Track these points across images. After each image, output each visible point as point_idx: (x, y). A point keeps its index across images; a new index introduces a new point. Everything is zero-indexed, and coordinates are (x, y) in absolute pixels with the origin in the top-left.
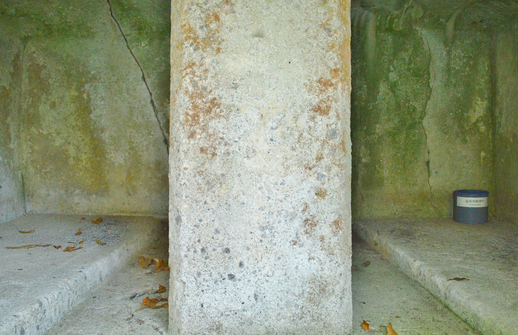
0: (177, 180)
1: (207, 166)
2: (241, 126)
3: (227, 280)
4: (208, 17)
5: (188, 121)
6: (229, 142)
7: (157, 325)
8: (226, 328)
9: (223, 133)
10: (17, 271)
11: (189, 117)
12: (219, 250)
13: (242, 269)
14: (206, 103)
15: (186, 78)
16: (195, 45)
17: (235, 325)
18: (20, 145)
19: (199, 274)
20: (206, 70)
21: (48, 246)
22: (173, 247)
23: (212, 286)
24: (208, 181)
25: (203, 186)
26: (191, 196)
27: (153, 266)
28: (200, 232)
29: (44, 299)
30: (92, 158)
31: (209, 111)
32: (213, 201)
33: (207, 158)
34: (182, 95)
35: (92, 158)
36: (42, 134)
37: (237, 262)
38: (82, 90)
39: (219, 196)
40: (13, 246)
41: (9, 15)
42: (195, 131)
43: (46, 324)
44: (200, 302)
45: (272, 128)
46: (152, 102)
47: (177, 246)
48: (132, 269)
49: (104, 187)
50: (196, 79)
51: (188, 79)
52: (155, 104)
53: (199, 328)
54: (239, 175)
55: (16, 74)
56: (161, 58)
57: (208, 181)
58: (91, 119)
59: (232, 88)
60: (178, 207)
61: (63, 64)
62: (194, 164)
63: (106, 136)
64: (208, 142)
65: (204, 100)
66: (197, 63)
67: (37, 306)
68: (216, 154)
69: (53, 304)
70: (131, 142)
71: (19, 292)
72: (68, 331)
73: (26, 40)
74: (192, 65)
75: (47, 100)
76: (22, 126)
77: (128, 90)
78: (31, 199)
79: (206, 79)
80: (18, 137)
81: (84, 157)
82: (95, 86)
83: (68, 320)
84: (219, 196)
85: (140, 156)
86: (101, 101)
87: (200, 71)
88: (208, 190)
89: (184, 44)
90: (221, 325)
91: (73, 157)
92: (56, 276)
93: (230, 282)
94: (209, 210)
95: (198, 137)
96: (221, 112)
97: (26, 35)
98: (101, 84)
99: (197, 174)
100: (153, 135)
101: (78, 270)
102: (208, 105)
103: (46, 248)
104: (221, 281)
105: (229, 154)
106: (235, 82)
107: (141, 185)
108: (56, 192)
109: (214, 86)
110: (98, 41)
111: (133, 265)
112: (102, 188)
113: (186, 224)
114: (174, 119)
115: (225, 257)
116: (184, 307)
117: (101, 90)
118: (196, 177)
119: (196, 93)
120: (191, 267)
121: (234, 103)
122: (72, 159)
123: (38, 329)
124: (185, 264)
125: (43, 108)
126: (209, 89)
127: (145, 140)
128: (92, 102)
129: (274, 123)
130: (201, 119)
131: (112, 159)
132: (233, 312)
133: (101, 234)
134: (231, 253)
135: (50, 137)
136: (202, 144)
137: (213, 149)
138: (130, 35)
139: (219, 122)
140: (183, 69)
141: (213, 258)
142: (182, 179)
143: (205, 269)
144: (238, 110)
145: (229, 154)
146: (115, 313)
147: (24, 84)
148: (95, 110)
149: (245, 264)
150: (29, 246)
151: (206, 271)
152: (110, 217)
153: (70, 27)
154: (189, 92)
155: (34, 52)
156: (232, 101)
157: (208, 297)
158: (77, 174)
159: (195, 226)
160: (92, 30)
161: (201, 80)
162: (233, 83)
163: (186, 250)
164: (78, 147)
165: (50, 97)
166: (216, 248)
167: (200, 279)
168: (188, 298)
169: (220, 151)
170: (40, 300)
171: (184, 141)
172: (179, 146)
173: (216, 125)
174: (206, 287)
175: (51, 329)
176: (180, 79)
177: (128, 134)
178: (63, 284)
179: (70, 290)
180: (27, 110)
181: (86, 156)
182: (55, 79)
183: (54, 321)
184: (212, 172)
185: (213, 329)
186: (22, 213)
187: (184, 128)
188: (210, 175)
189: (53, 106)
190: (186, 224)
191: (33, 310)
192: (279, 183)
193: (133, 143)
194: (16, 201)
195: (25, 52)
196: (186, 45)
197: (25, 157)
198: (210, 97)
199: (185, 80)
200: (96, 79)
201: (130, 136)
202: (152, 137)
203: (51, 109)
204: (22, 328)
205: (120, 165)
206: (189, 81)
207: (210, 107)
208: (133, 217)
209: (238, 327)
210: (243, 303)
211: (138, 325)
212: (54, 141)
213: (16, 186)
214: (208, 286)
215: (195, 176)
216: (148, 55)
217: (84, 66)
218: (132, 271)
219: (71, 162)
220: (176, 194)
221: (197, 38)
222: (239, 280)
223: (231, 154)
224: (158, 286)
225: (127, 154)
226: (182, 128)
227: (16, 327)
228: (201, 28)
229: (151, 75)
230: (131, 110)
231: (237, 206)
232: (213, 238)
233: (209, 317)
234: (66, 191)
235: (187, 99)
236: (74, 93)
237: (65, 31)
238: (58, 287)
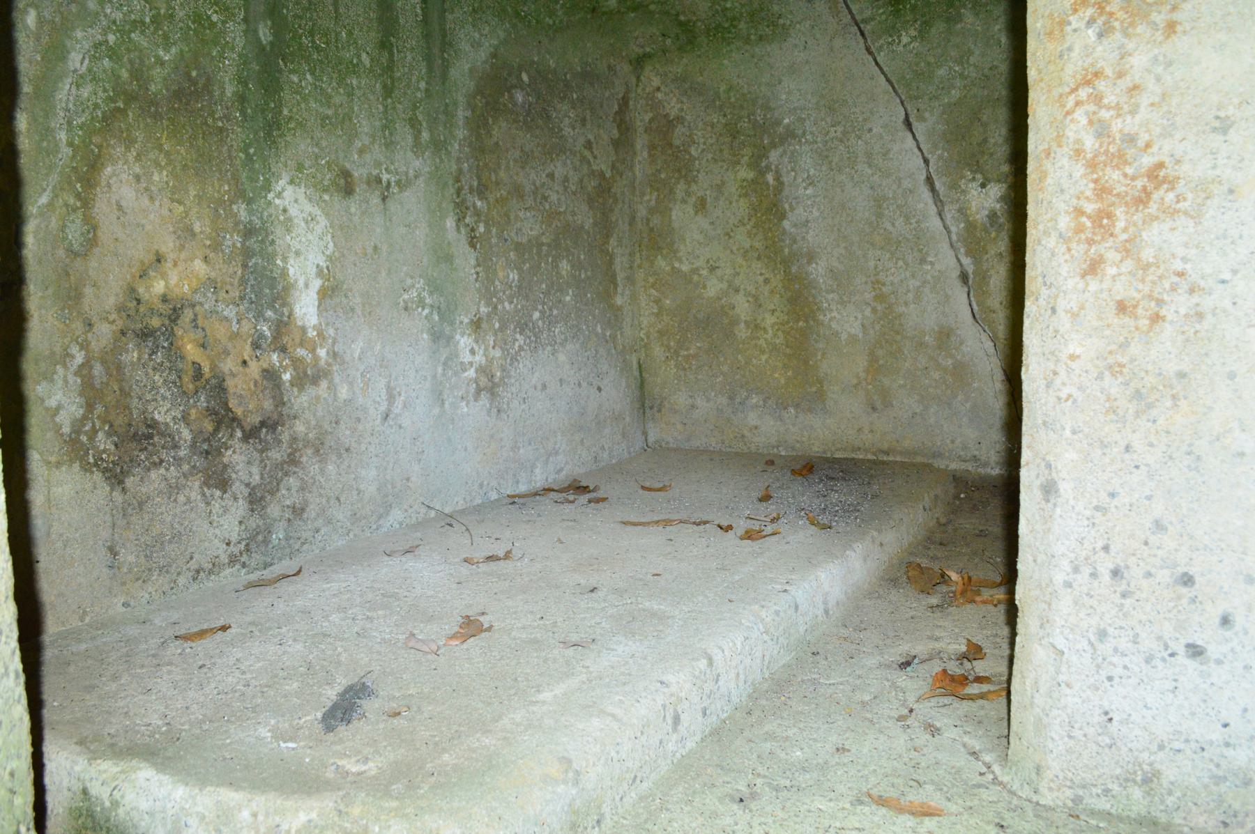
0: (1048, 387)
1: (1135, 349)
2: (1241, 237)
3: (1182, 659)
5: (1082, 231)
6: (1202, 283)
7: (976, 745)
8: (1172, 783)
9: (1185, 260)
10: (649, 576)
11: (1084, 219)
12: (1164, 576)
13: (1228, 634)
14: (1133, 178)
15: (1076, 115)
16: (1100, 22)
17: (1199, 778)
18: (634, 297)
19: (1102, 634)
20: (1135, 87)
21: (705, 523)
22: (1031, 559)
23: (1137, 669)
24: (1137, 391)
26: (1086, 430)
27: (944, 588)
28: (1110, 524)
29: (716, 651)
30: (788, 323)
31: (1142, 200)
32: (1151, 445)
33: (1137, 329)
34: (1065, 161)
35: (788, 323)
36: (679, 271)
37: (1215, 613)
38: (763, 164)
39: (1168, 432)
40: (633, 519)
41: (604, 13)
42: (1101, 256)
43: (719, 706)
44: (1101, 707)
46: (929, 180)
47: (1041, 558)
48: (894, 592)
49: (814, 389)
50: (1105, 114)
51: (1080, 116)
52: (938, 185)
53: (1096, 773)
54: (1232, 376)
55: (623, 143)
56: (950, 68)
57: (1137, 391)
58: (784, 232)
59: (1215, 130)
60: (1050, 458)
61: (721, 108)
63: (818, 271)
64: (1141, 286)
66: (1109, 72)
67: (703, 663)
68: (1163, 319)
69: (734, 664)
70: (878, 282)
71: (661, 627)
72: (766, 729)
73: (639, 62)
74: (1091, 77)
75: (688, 193)
76: (638, 255)
77: (869, 155)
78: (657, 415)
79: (1133, 113)
80: (630, 280)
81: (770, 320)
82: (792, 153)
83: (764, 702)
84: (1168, 432)
85: (900, 315)
86: (805, 188)
87: (1118, 91)
88: (1137, 414)
89: (1069, 24)
90: (1157, 774)
91: (746, 322)
92: (733, 597)
93: (1192, 664)
94: (1137, 467)
95: (1112, 271)
96: (1178, 202)
97: (640, 51)
98: (806, 148)
99: (1107, 373)
100: (932, 263)
101: (778, 587)
102: (1139, 184)
103: (702, 527)
104: (1164, 660)
105: (1200, 316)
106: (1222, 114)
107: (901, 386)
108: (708, 400)
109: (1158, 130)
110: (796, 46)
111: (894, 582)
112: (808, 390)
113: (1072, 502)
114: (1041, 227)
115: (1179, 598)
116: (1055, 712)
117: (807, 162)
118: (1102, 379)
119: (1107, 151)
120: (1082, 615)
121: (1218, 172)
122: (742, 325)
123: (705, 714)
124: (1065, 604)
125: (680, 214)
126: (1144, 138)
127: (913, 276)
128: (786, 192)
130: (1120, 224)
131: (834, 325)
132: (1193, 745)
133: (817, 501)
134: (1197, 586)
135: (696, 278)
136: (1122, 290)
137: (1153, 304)
138: (873, 19)
139: (1173, 229)
140: (1067, 90)
141: (1144, 595)
142: (1064, 384)
143: (1119, 623)
144: (1231, 191)
145: (1200, 316)
146: (867, 698)
147: (640, 162)
148: (792, 209)
149: (1239, 620)
150: (667, 523)
151: (1121, 628)
152: (833, 462)
153: (734, 19)
154: (1084, 151)
155: (658, 89)
156: (1214, 167)
157: (1125, 697)
158: (754, 361)
159: (1097, 508)
160: (781, 21)
161: (1119, 115)
162: (1217, 118)
163: (1069, 570)
164: (756, 298)
165: (694, 187)
166: (1153, 571)
167: (1106, 648)
168: (1068, 691)
169: (1173, 308)
170: (709, 651)
171: (1070, 283)
172: (1056, 297)
173: (1163, 237)
174: (1120, 671)
175: (729, 718)
176: (1060, 117)
177: (872, 264)
178: (752, 618)
179: (766, 632)
180: (648, 220)
182: (705, 143)
183: (735, 700)
184: (1150, 367)
185: (1135, 781)
186: (639, 444)
187: (1069, 250)
188: (1143, 374)
189: (701, 206)
190: (1072, 502)
191: (697, 673)
193: (884, 284)
194: (628, 419)
196: (1074, 25)
198: (1147, 161)
199: (1072, 121)
200: (794, 136)
201: (876, 267)
203: (696, 213)
204: (675, 711)
205: (853, 339)
206: (1084, 121)
207: (1144, 189)
208: (883, 463)
209: (1206, 787)
210: (1226, 726)
211: (928, 737)
212: (704, 287)
213: (628, 386)
214: (1125, 667)
215: (1100, 377)
216: (917, 64)
217: (766, 107)
218: (894, 595)
219: (742, 332)
220: (1045, 423)
222: (1219, 662)
223: (1209, 316)
224: (965, 641)
225: (868, 312)
226: (1064, 248)
227: (664, 706)
229: (927, 115)
230: (879, 202)
231: (1223, 461)
232: (1146, 543)
233: (1124, 749)
234: (731, 398)
235: (1079, 170)
236: (746, 173)
237: (722, 31)
238: (741, 623)
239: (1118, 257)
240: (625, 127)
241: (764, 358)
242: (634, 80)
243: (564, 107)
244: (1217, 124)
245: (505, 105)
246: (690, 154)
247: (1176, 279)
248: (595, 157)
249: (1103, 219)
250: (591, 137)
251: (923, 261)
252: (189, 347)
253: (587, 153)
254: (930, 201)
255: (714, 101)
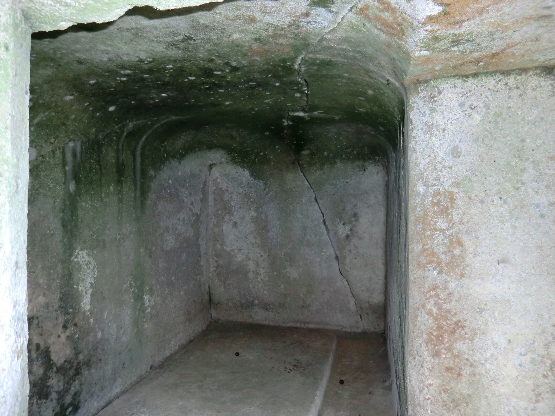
4: (451, 242)
9: (468, 355)
20: (450, 294)
25: (449, 403)
31: (453, 332)
45: (521, 354)
46: (324, 222)
50: (441, 302)
51: (431, 300)
52: (327, 224)
62: (439, 381)
65: (449, 322)
66: (441, 287)
68: (462, 375)
74: (435, 288)
81: (262, 271)
100: (325, 252)
102: (452, 327)
105: (475, 375)
122: (251, 273)
129: (523, 349)
130: (446, 340)
131: (288, 274)
135: (233, 253)
145: (475, 375)
161: (445, 303)
162: (478, 308)
165: (232, 218)
173: (461, 346)
181: (264, 271)
184: (458, 391)
189: (235, 224)
192: (529, 409)
195: (210, 178)
197: (211, 270)
198: (455, 319)
202: (324, 254)
203: (233, 227)
206: (433, 303)
207: (454, 328)
212: (236, 257)
215: (440, 393)
219: (251, 275)
221: (440, 262)
228: (444, 253)
236: (253, 214)
239: (445, 352)
240: (205, 193)
241: (260, 285)
242: (208, 173)
243: (183, 190)
244: (478, 310)
245: (163, 195)
246: (230, 204)
247: (466, 361)
248: (194, 208)
249: (440, 338)
250: (193, 200)
251: (322, 251)
252: (35, 337)
253: (191, 207)
254: (324, 229)
255: (240, 184)
